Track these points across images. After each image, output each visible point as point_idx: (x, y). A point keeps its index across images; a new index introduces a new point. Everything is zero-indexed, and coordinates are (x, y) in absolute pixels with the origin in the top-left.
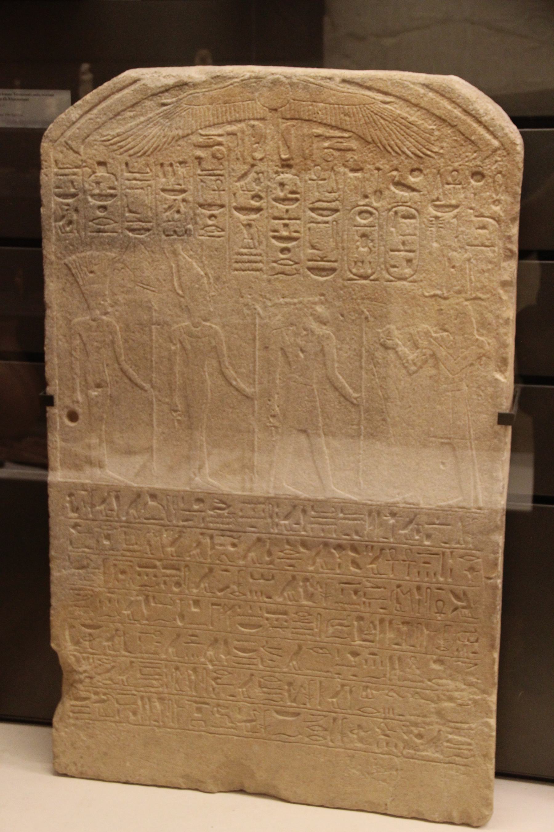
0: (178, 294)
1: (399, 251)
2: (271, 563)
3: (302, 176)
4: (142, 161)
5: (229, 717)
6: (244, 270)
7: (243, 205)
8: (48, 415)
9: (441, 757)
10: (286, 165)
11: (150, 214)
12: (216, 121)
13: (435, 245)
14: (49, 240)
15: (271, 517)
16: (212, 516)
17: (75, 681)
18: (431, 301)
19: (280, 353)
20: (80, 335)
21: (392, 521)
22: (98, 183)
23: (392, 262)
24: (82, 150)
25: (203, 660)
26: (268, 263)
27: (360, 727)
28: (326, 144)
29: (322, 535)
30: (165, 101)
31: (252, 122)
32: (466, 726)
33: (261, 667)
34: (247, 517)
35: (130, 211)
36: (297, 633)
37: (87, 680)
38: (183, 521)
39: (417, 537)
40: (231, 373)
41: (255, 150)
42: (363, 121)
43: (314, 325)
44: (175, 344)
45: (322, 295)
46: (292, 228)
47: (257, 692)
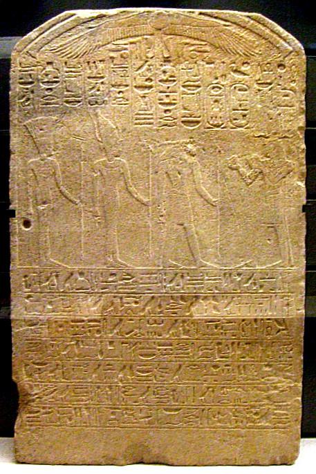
0: (98, 141)
2: (161, 312)
3: (177, 67)
6: (141, 124)
7: (140, 85)
10: (167, 60)
11: (80, 92)
12: (123, 36)
13: (260, 106)
16: (122, 284)
19: (165, 175)
20: (32, 170)
23: (234, 117)
24: (37, 55)
26: (157, 119)
28: (192, 48)
29: (195, 291)
30: (90, 26)
31: (145, 37)
36: (179, 357)
39: (255, 288)
40: (132, 189)
42: (213, 36)
43: (186, 157)
44: (96, 173)
45: (191, 138)
46: (172, 98)
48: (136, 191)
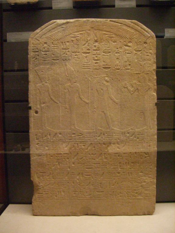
0: (67, 76)
1: (127, 62)
2: (95, 150)
4: (57, 42)
5: (83, 195)
8: (29, 112)
9: (142, 198)
10: (96, 41)
11: (59, 55)
12: (77, 31)
13: (136, 60)
14: (30, 64)
15: (95, 137)
17: (38, 189)
18: (136, 75)
21: (128, 135)
22: (44, 48)
23: (125, 65)
24: (40, 40)
25: (76, 179)
27: (120, 193)
28: (107, 36)
29: (109, 140)
30: (63, 27)
31: (87, 31)
32: (148, 188)
33: (92, 180)
34: (87, 137)
35: (53, 55)
36: (103, 169)
37: (42, 188)
38: (69, 140)
40: (82, 97)
41: (88, 38)
42: (116, 30)
43: (105, 82)
46: (98, 57)
47: (92, 187)
48: (83, 97)
